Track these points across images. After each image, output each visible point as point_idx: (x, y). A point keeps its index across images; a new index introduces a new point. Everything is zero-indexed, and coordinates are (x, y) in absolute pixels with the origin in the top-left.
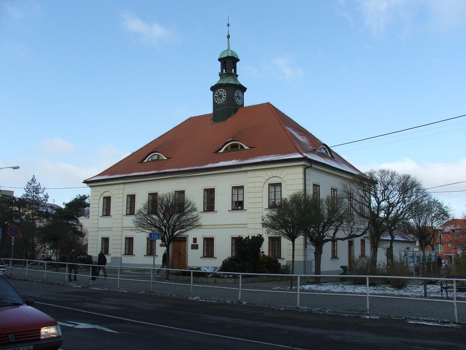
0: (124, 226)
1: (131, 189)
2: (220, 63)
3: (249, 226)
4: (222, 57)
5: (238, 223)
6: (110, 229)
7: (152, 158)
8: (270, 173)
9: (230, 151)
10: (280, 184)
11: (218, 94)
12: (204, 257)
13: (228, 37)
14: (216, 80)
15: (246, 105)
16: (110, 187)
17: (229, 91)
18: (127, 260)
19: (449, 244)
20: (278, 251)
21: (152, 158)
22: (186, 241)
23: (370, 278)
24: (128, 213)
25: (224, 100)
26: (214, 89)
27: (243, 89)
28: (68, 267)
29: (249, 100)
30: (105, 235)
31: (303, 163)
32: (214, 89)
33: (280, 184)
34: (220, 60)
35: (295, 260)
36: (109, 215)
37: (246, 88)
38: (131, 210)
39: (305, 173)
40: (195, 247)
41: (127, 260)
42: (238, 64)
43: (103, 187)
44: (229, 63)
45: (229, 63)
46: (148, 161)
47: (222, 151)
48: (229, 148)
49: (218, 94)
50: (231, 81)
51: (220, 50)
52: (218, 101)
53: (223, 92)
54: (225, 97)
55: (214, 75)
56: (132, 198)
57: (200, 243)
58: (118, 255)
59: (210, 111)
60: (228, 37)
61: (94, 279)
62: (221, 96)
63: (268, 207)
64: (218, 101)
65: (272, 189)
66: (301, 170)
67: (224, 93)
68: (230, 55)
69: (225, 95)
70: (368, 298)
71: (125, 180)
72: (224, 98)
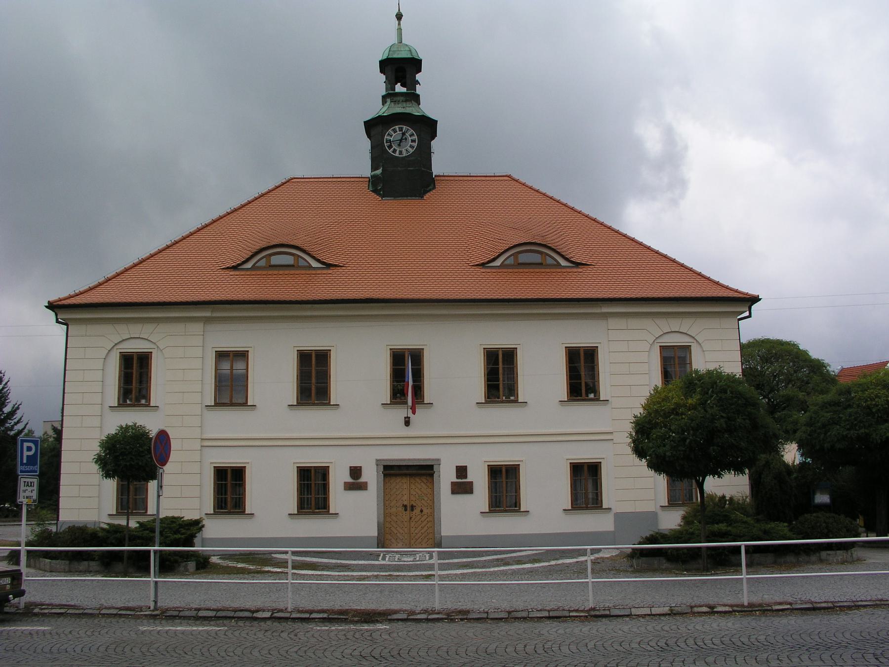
0: (204, 436)
4: (395, 56)
7: (516, 258)
8: (125, 331)
22: (432, 475)
29: (444, 159)
40: (462, 487)
44: (401, 69)
45: (401, 69)
46: (503, 266)
57: (371, 475)
72: (411, 147)
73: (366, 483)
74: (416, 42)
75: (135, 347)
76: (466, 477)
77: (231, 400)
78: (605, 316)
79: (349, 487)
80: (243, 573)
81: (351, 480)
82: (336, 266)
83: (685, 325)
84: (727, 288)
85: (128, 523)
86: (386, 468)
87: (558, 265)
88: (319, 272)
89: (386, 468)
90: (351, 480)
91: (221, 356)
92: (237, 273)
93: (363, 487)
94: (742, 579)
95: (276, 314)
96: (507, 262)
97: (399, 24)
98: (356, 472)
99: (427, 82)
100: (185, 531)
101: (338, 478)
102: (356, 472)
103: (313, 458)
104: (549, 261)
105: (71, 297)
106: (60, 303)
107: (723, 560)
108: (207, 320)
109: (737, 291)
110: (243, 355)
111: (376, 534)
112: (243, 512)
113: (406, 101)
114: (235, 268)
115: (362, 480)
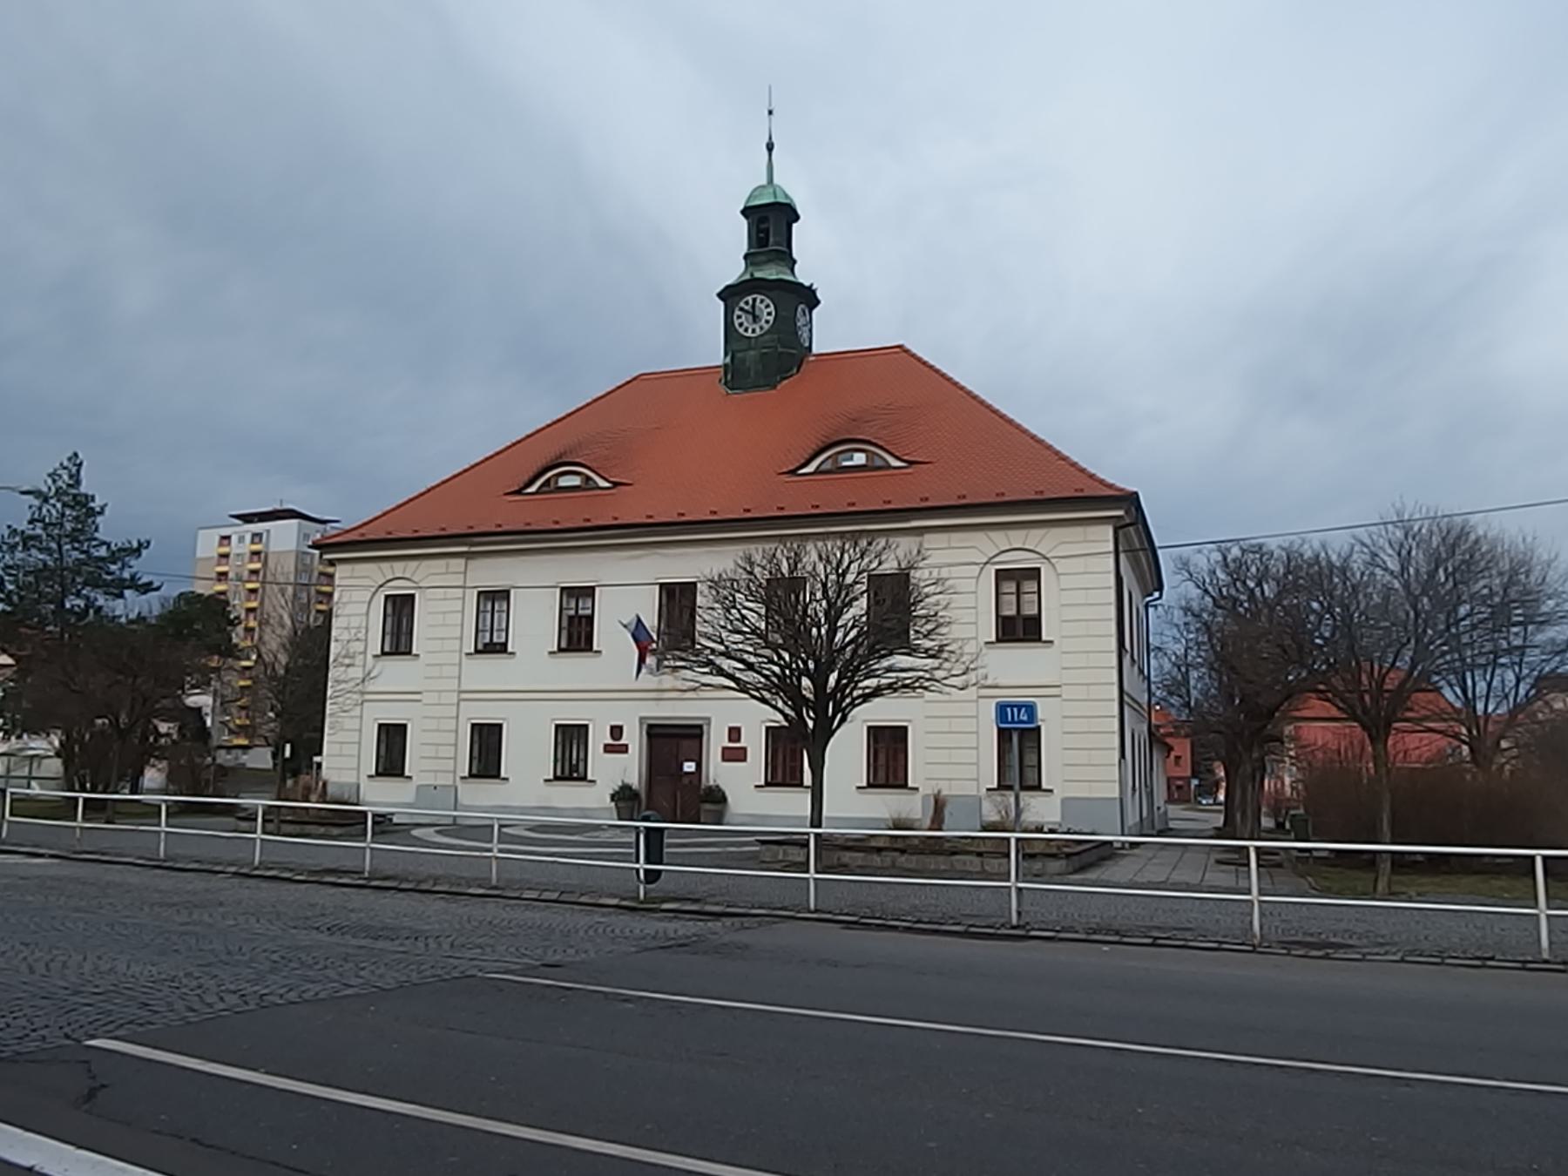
0: (463, 688)
1: (577, 569)
2: (744, 223)
3: (1066, 692)
7: (836, 461)
8: (1001, 539)
10: (1035, 574)
11: (753, 306)
13: (770, 147)
14: (734, 270)
15: (815, 350)
16: (413, 564)
18: (481, 798)
19: (693, 765)
22: (701, 736)
25: (766, 327)
27: (809, 298)
29: (829, 333)
32: (729, 295)
33: (1035, 574)
34: (746, 212)
35: (807, 798)
40: (735, 755)
41: (481, 798)
43: (385, 565)
44: (771, 223)
45: (771, 223)
46: (817, 472)
47: (533, 489)
49: (753, 306)
50: (770, 273)
51: (744, 184)
54: (771, 318)
57: (634, 738)
60: (770, 147)
66: (1108, 531)
68: (782, 200)
73: (744, 749)
74: (795, 187)
79: (608, 749)
80: (1451, 872)
83: (1033, 538)
84: (1102, 482)
86: (650, 726)
87: (889, 467)
89: (650, 726)
91: (568, 592)
93: (624, 749)
94: (807, 879)
96: (824, 467)
98: (616, 731)
99: (802, 237)
101: (598, 738)
102: (616, 731)
103: (572, 714)
108: (468, 556)
109: (1111, 486)
110: (589, 592)
112: (497, 776)
113: (769, 261)
114: (519, 492)
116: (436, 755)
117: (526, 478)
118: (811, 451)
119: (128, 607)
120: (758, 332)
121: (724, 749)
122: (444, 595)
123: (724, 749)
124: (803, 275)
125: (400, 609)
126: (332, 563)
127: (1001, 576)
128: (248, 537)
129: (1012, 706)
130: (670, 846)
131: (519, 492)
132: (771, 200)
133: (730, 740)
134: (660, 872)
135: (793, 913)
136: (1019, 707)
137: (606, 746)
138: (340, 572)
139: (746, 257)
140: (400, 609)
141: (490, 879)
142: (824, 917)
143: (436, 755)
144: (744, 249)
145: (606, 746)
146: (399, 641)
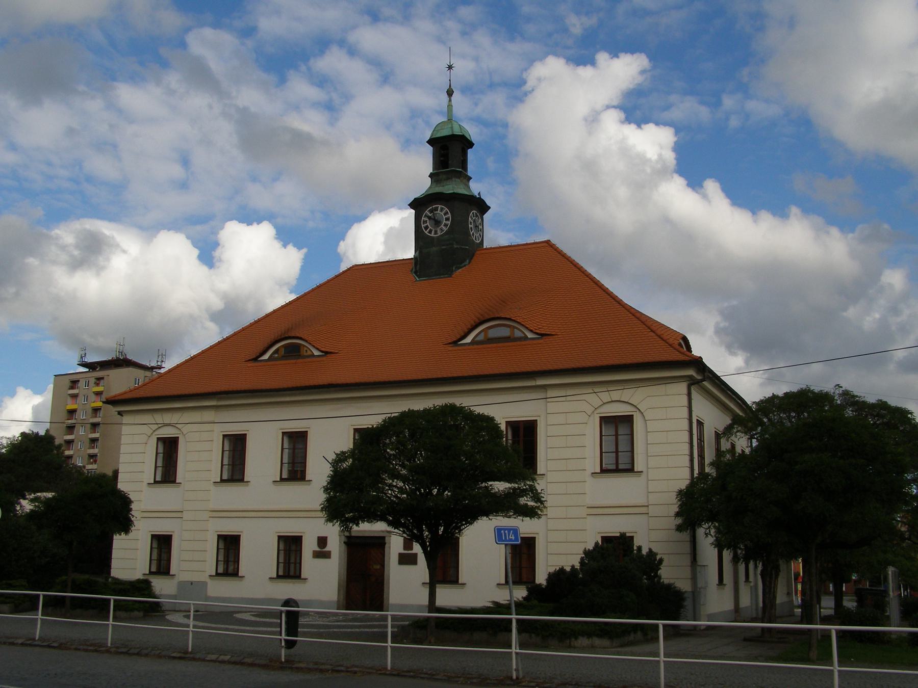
2: (430, 149)
3: (186, 516)
4: (439, 135)
5: (241, 508)
6: (177, 514)
9: (284, 357)
12: (278, 577)
15: (486, 245)
17: (449, 210)
20: (295, 564)
21: (486, 335)
23: (115, 600)
24: (158, 478)
25: (445, 229)
26: (418, 205)
28: (520, 631)
29: (496, 234)
30: (229, 527)
31: (691, 372)
32: (418, 205)
34: (431, 142)
36: (174, 481)
37: (489, 208)
38: (295, 472)
39: (689, 395)
41: (223, 590)
42: (470, 153)
44: (450, 151)
46: (473, 342)
47: (266, 357)
48: (282, 352)
50: (450, 188)
52: (430, 232)
53: (443, 212)
54: (449, 223)
55: (417, 171)
56: (297, 441)
58: (204, 577)
59: (410, 253)
61: (290, 644)
62: (437, 223)
63: (598, 470)
64: (430, 232)
65: (609, 431)
67: (446, 213)
68: (457, 132)
69: (447, 219)
70: (662, 665)
71: (220, 399)
72: (446, 225)
75: (235, 429)
76: (412, 549)
77: (617, 466)
78: (544, 387)
79: (318, 555)
81: (318, 549)
82: (331, 353)
83: (627, 394)
85: (511, 592)
87: (526, 338)
88: (535, 342)
90: (318, 549)
92: (456, 348)
93: (327, 555)
94: (659, 661)
95: (220, 403)
97: (450, 100)
100: (142, 587)
101: (309, 546)
104: (518, 334)
105: (125, 393)
106: (120, 398)
107: (563, 636)
111: (427, 603)
113: (448, 179)
114: (255, 359)
115: (327, 549)
116: (194, 559)
117: (261, 348)
118: (469, 327)
119: (162, 371)
120: (439, 234)
121: (400, 554)
122: (201, 440)
123: (400, 554)
124: (476, 188)
125: (169, 449)
126: (120, 413)
127: (605, 420)
128: (93, 381)
129: (505, 530)
130: (304, 626)
131: (255, 359)
132: (450, 133)
133: (405, 548)
134: (296, 641)
135: (98, 648)
136: (509, 530)
137: (314, 552)
138: (126, 419)
139: (431, 176)
140: (169, 449)
141: (386, 669)
142: (47, 644)
143: (194, 559)
144: (430, 169)
145: (314, 552)
146: (168, 472)
